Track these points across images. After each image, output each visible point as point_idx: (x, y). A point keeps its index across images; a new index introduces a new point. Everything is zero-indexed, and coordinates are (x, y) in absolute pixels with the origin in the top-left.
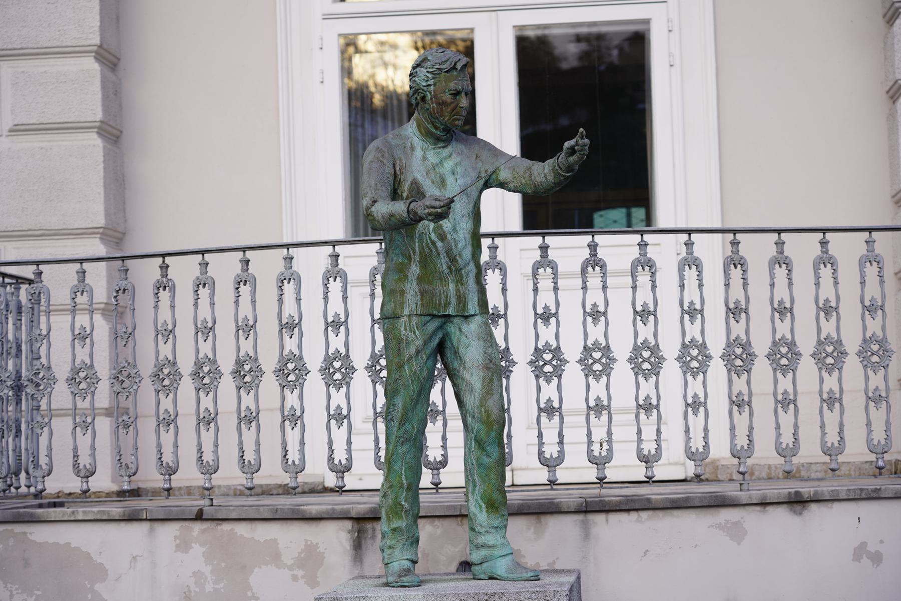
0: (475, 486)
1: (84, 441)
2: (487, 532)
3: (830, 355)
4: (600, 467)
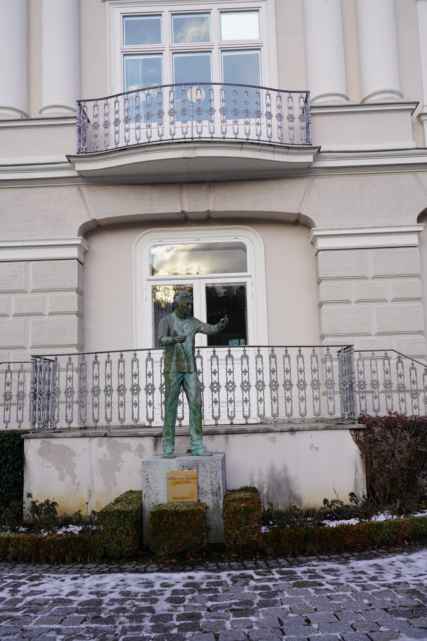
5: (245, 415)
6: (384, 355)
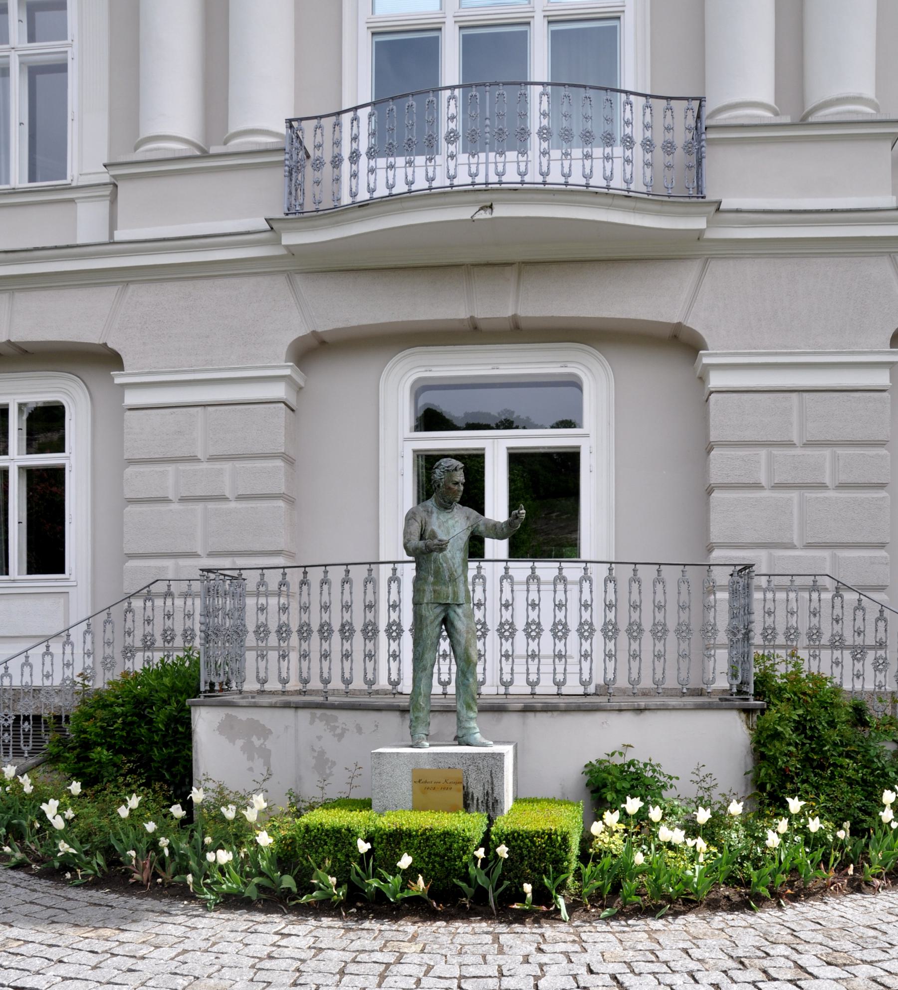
1: (262, 664)
3: (660, 631)
5: (505, 680)
6: (812, 583)
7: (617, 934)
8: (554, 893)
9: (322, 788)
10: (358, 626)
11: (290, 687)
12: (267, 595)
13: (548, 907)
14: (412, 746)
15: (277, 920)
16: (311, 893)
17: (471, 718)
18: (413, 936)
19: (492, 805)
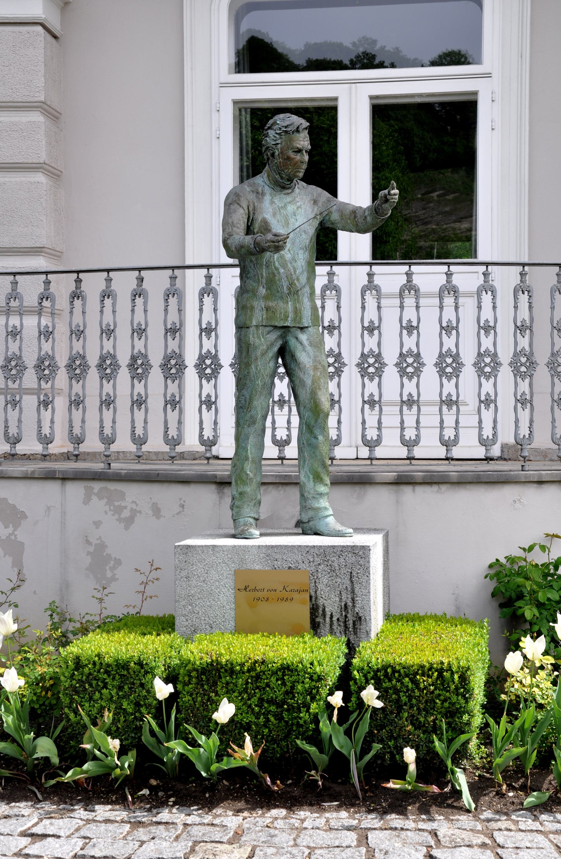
0: (305, 461)
2: (313, 497)
4: (410, 448)
7: (551, 836)
8: (449, 763)
9: (101, 600)
10: (156, 358)
11: (54, 448)
12: (21, 312)
13: (441, 787)
14: (234, 536)
15: (26, 812)
16: (81, 766)
17: (321, 494)
18: (236, 833)
19: (352, 625)
